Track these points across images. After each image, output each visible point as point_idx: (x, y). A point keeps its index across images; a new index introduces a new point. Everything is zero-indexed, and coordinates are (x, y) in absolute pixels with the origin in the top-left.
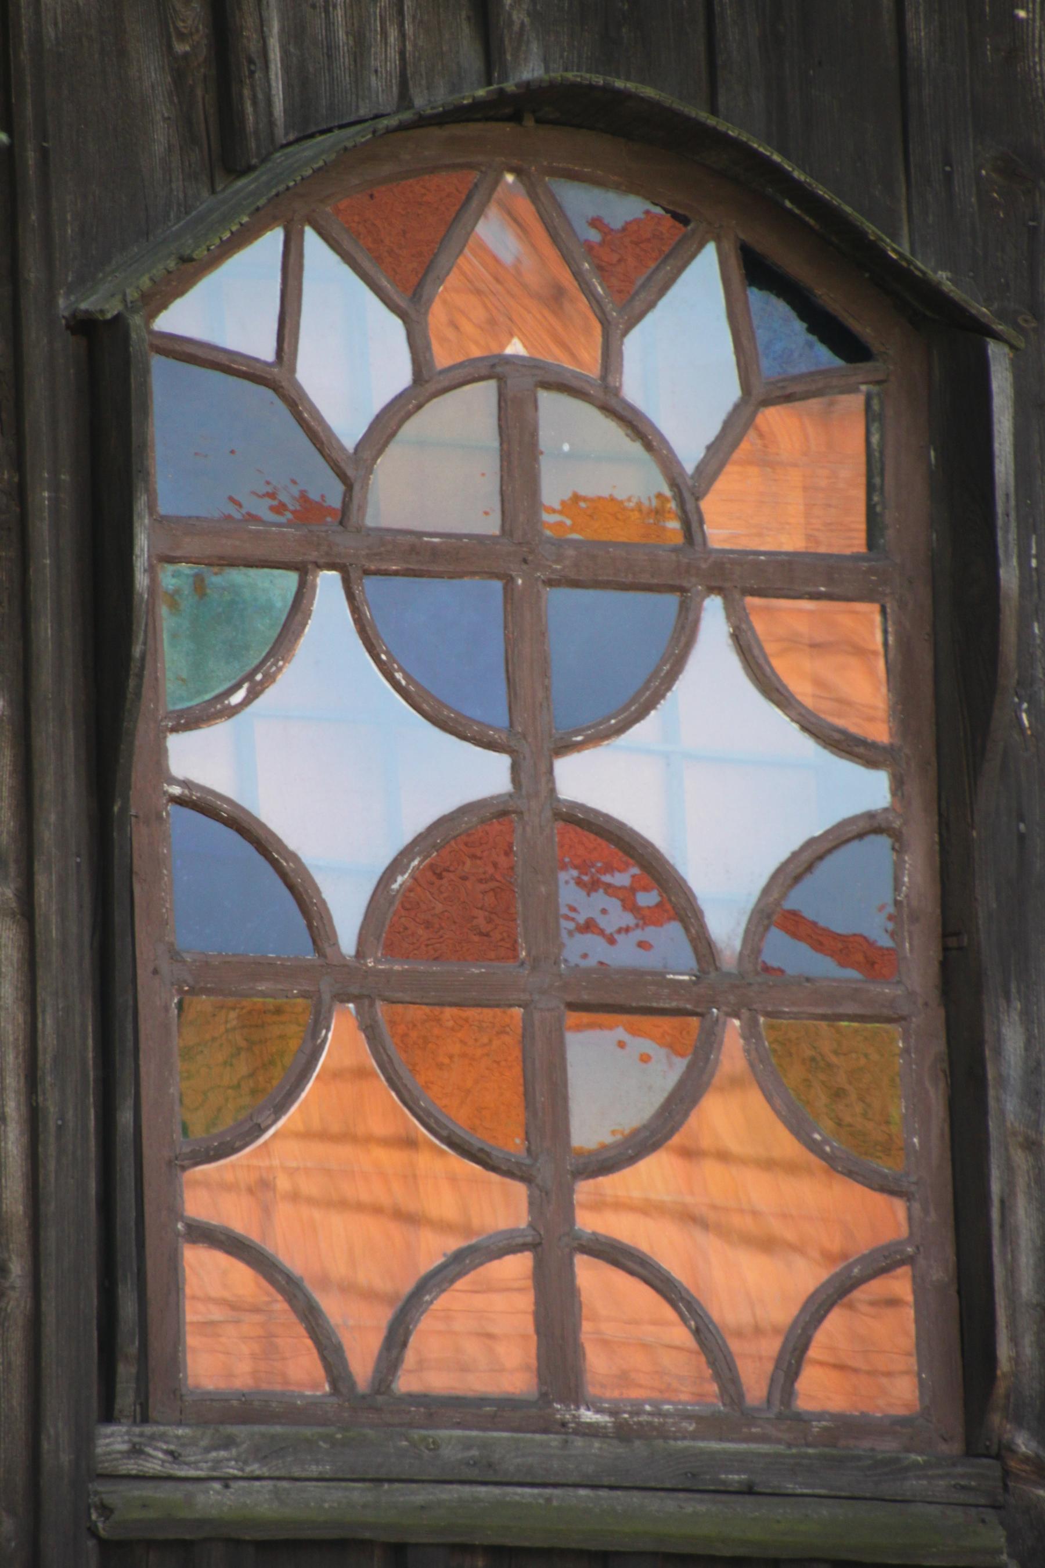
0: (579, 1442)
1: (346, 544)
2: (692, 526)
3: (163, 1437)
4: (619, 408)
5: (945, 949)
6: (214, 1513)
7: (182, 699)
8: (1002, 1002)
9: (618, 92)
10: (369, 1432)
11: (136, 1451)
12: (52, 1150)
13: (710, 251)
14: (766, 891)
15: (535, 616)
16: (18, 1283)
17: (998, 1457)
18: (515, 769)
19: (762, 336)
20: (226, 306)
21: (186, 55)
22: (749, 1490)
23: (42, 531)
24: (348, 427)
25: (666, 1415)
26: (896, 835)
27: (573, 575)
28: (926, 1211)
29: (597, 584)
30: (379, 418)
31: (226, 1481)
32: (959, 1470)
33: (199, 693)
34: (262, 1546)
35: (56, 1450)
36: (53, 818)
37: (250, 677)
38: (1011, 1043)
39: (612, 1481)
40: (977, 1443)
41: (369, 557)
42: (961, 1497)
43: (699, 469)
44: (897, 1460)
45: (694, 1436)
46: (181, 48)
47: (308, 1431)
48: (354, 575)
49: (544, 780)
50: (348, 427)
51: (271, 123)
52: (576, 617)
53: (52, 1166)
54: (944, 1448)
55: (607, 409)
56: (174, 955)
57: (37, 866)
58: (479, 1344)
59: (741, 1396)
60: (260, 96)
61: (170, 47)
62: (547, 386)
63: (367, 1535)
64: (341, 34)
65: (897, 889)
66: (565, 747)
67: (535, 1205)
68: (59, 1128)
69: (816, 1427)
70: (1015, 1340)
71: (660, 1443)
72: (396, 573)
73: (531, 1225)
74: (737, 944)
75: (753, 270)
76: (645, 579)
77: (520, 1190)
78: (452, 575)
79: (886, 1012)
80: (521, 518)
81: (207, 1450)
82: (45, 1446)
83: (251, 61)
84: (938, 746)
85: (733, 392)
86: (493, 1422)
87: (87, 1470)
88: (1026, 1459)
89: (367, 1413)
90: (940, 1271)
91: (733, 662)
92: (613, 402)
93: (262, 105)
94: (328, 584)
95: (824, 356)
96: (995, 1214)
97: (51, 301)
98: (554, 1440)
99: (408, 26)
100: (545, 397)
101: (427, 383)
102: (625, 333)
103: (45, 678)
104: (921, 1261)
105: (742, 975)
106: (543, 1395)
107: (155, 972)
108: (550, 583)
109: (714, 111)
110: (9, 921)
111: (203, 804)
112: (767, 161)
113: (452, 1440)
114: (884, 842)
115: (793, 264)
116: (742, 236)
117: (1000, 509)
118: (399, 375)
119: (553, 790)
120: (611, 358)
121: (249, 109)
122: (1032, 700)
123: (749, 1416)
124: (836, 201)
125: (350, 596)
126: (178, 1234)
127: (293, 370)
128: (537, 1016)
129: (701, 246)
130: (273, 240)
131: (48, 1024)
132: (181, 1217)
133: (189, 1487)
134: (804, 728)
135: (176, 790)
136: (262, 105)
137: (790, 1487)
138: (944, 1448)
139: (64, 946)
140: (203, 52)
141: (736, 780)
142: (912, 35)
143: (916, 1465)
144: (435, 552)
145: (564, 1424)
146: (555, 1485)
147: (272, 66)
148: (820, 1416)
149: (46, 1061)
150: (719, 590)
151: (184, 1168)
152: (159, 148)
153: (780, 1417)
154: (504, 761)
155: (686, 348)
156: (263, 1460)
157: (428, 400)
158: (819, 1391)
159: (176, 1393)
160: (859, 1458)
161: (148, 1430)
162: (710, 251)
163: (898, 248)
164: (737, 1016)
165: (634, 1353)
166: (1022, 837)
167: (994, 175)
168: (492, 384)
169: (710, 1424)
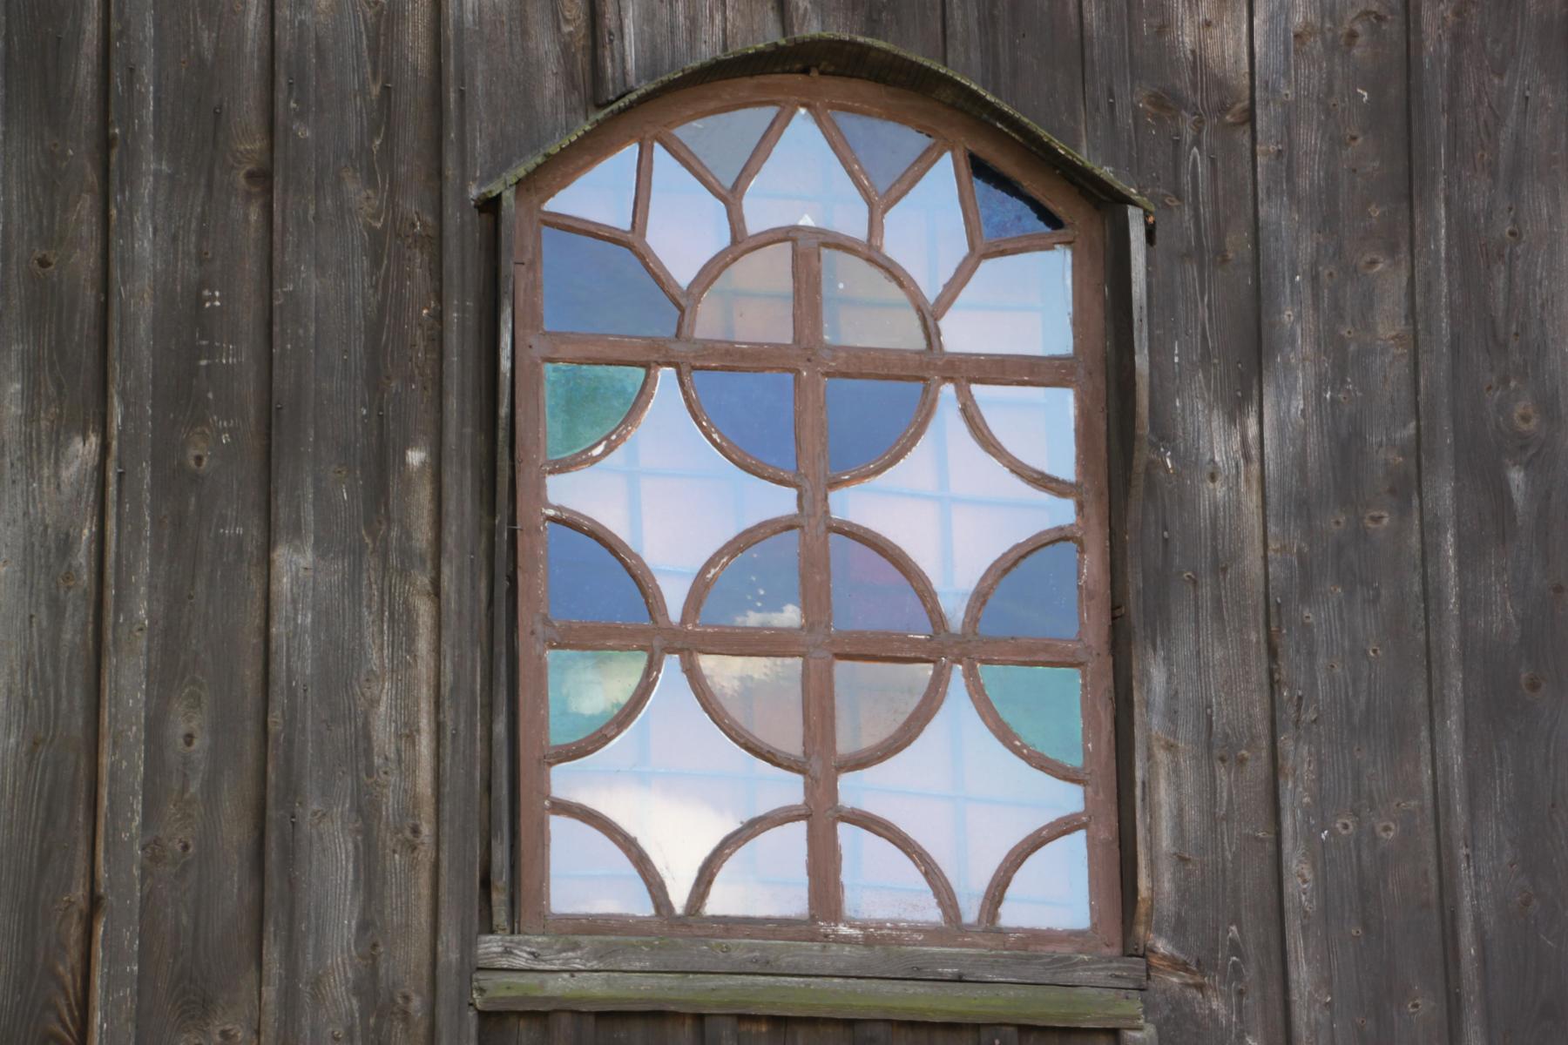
0: (834, 947)
1: (679, 349)
2: (931, 334)
3: (527, 943)
4: (880, 260)
5: (1114, 618)
6: (558, 993)
7: (558, 453)
8: (1150, 651)
9: (861, 45)
10: (680, 941)
11: (507, 952)
12: (449, 750)
13: (947, 160)
14: (983, 579)
15: (819, 402)
16: (427, 840)
17: (1143, 956)
18: (800, 498)
19: (983, 212)
20: (596, 194)
21: (570, 34)
22: (959, 979)
23: (453, 339)
24: (683, 273)
25: (902, 929)
26: (1080, 542)
27: (844, 369)
28: (1097, 793)
29: (861, 376)
30: (705, 267)
31: (572, 972)
32: (1115, 965)
33: (570, 448)
34: (600, 1016)
35: (450, 954)
36: (454, 529)
37: (607, 438)
38: (1155, 678)
39: (858, 973)
40: (1131, 948)
41: (695, 358)
42: (1116, 983)
43: (938, 300)
44: (1069, 958)
45: (922, 944)
46: (567, 29)
47: (633, 940)
48: (685, 369)
49: (820, 505)
50: (683, 273)
51: (624, 73)
52: (849, 399)
53: (448, 761)
54: (1107, 951)
55: (870, 260)
56: (546, 621)
57: (443, 561)
58: (765, 886)
59: (958, 916)
60: (617, 56)
61: (559, 28)
62: (827, 245)
63: (672, 1008)
64: (681, 18)
65: (1079, 578)
66: (835, 484)
67: (809, 790)
68: (454, 736)
69: (1012, 938)
70: (1154, 876)
71: (895, 948)
72: (715, 369)
73: (806, 803)
74: (961, 615)
75: (979, 168)
76: (896, 371)
77: (798, 779)
78: (756, 370)
79: (1069, 659)
80: (807, 331)
81: (560, 952)
82: (440, 948)
83: (610, 33)
84: (1109, 481)
85: (965, 250)
86: (774, 935)
87: (472, 968)
88: (1164, 957)
89: (682, 928)
90: (1107, 832)
91: (962, 427)
92: (875, 256)
93: (618, 60)
94: (666, 374)
95: (1042, 227)
96: (1138, 792)
97: (463, 189)
98: (816, 946)
99: (729, 13)
100: (825, 252)
101: (741, 244)
102: (885, 211)
103: (451, 438)
104: (1092, 826)
105: (964, 635)
106: (812, 917)
107: (533, 633)
108: (827, 374)
109: (945, 64)
110: (425, 599)
111: (570, 522)
112: (967, 89)
113: (741, 948)
114: (1072, 546)
115: (1006, 164)
116: (974, 149)
117: (1136, 317)
118: (721, 238)
119: (827, 512)
120: (875, 225)
121: (609, 64)
122: (1174, 450)
123: (965, 930)
124: (1017, 115)
125: (682, 384)
126: (544, 808)
127: (643, 235)
128: (812, 662)
129: (940, 154)
130: (631, 152)
131: (448, 666)
132: (548, 797)
133: (545, 976)
134: (1012, 471)
135: (551, 512)
136: (618, 60)
137: (989, 977)
138: (1107, 951)
139: (460, 614)
140: (583, 32)
141: (968, 501)
142: (1087, 16)
143: (1084, 962)
144: (743, 355)
145: (826, 936)
146: (817, 976)
147: (627, 37)
148: (1016, 930)
149: (445, 691)
150: (951, 379)
151: (550, 765)
152: (548, 93)
153: (986, 931)
154: (793, 492)
155: (932, 217)
156: (601, 958)
157: (742, 255)
158: (1015, 914)
159: (542, 913)
160: (1041, 957)
161: (516, 938)
162: (947, 160)
163: (1083, 156)
164: (960, 662)
165: (880, 890)
166: (1166, 541)
167: (1149, 107)
168: (788, 245)
169: (932, 934)
